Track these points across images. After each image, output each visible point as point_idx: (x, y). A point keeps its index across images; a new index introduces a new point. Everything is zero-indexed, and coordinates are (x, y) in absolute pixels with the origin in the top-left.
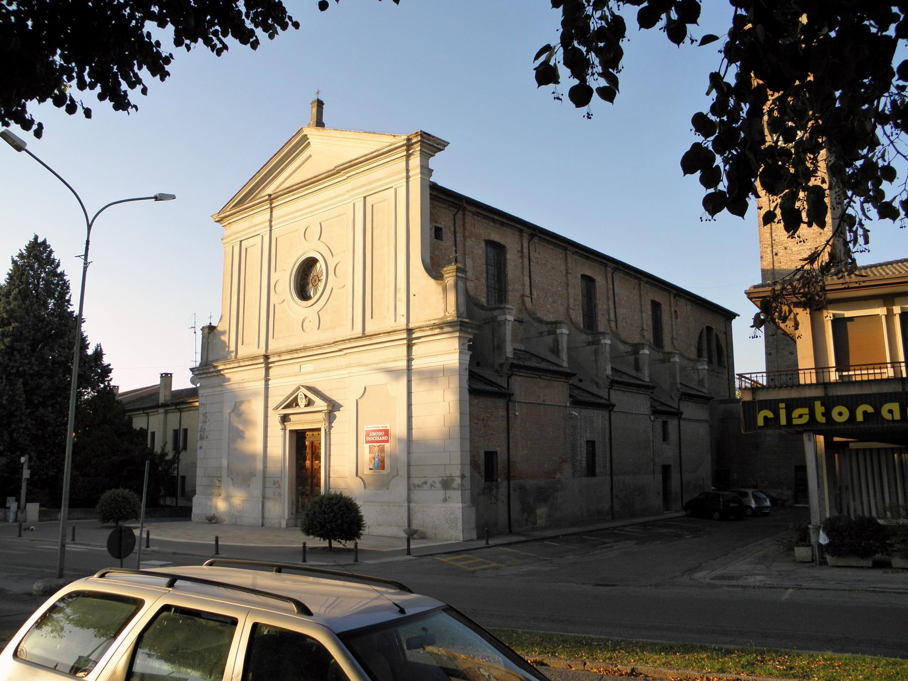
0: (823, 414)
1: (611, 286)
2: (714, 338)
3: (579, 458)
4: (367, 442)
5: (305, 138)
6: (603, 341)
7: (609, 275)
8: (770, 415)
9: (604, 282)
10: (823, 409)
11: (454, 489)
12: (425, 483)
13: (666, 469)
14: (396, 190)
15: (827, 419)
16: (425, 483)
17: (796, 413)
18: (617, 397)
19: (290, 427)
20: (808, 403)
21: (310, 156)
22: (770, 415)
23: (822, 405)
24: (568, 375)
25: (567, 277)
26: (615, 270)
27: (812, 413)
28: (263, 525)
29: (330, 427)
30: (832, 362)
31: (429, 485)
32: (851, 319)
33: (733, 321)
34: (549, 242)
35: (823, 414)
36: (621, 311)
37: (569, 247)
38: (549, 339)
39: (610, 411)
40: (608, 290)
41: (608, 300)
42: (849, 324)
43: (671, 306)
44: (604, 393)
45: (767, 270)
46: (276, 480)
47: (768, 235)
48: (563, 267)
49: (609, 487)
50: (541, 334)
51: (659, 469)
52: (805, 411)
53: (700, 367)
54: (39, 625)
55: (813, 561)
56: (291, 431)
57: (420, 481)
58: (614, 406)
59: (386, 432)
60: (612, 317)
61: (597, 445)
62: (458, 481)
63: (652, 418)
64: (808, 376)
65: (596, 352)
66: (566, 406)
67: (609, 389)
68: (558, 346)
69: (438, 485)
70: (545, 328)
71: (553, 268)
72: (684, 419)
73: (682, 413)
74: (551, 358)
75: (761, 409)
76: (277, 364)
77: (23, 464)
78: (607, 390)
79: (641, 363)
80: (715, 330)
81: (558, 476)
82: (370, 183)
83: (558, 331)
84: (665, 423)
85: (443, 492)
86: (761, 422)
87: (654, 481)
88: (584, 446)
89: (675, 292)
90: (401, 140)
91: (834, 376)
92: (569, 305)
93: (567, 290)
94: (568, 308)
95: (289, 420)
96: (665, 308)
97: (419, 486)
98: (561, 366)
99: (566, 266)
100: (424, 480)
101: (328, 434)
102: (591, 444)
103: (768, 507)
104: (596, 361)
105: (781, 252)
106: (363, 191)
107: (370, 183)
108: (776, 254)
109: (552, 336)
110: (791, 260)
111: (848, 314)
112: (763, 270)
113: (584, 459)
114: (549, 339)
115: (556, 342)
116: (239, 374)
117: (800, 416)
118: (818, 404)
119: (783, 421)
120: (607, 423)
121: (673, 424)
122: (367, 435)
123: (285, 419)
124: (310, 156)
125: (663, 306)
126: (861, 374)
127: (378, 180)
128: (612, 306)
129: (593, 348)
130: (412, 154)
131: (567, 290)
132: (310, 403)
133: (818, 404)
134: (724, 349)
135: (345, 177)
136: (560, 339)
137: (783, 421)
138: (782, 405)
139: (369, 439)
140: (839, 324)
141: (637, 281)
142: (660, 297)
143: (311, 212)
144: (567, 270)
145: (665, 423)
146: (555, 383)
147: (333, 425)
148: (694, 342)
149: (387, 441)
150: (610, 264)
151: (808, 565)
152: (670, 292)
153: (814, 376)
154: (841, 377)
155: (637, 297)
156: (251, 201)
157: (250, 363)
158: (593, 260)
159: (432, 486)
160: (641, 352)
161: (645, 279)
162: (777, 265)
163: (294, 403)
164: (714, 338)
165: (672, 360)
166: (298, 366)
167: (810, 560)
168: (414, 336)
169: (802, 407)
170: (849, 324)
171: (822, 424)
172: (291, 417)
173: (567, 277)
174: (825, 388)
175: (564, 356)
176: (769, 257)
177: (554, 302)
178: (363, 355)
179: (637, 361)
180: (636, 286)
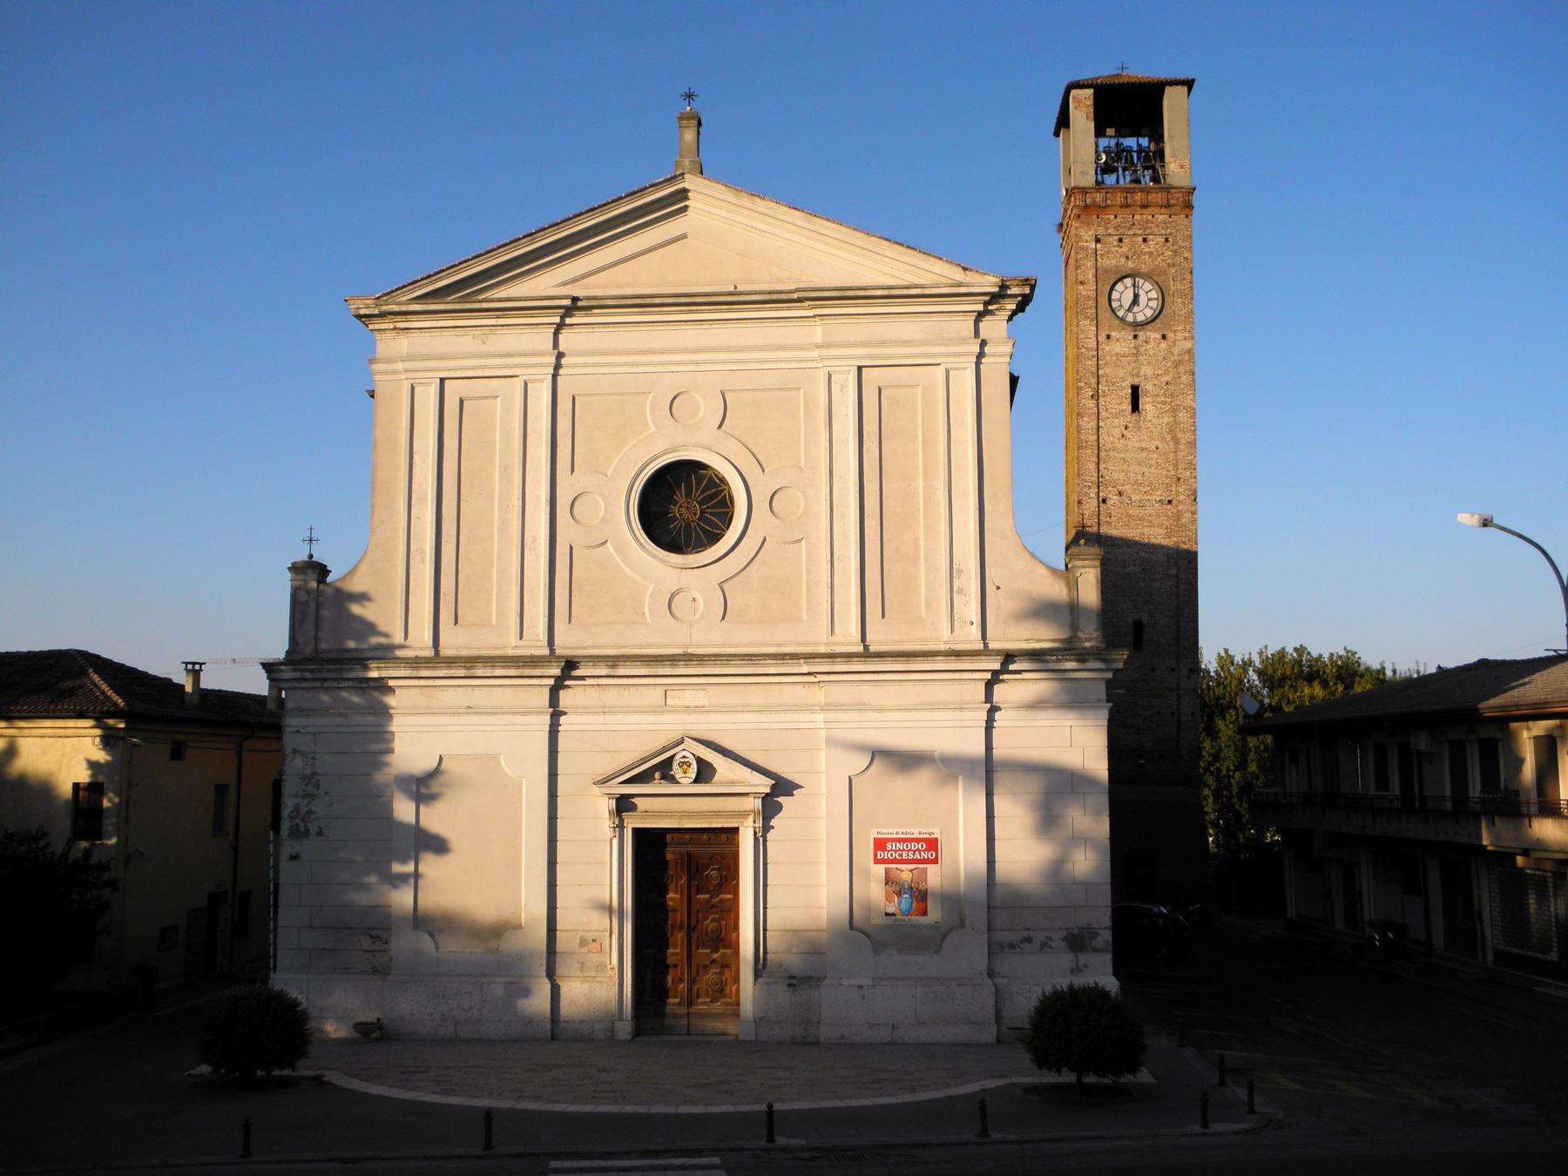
4: (877, 861)
5: (683, 194)
11: (1096, 950)
12: (1029, 940)
14: (947, 371)
16: (1029, 940)
19: (632, 822)
21: (684, 236)
28: (553, 1038)
29: (767, 828)
31: (1036, 944)
46: (589, 936)
54: (1555, 894)
56: (636, 831)
57: (1015, 937)
59: (932, 844)
62: (1107, 936)
69: (1061, 944)
76: (589, 681)
77: (1205, 798)
82: (883, 343)
85: (1072, 956)
90: (989, 284)
95: (633, 808)
97: (1011, 946)
100: (1026, 934)
101: (761, 839)
105: (1113, 499)
106: (862, 355)
107: (883, 343)
108: (1104, 501)
116: (450, 693)
122: (880, 844)
123: (624, 805)
124: (684, 236)
127: (905, 343)
130: (991, 313)
132: (705, 772)
135: (811, 313)
139: (881, 855)
143: (696, 363)
147: (772, 823)
149: (935, 861)
156: (462, 300)
157: (462, 672)
159: (1043, 945)
163: (664, 769)
166: (660, 691)
168: (1012, 667)
172: (635, 800)
176: (1091, 505)
178: (866, 688)
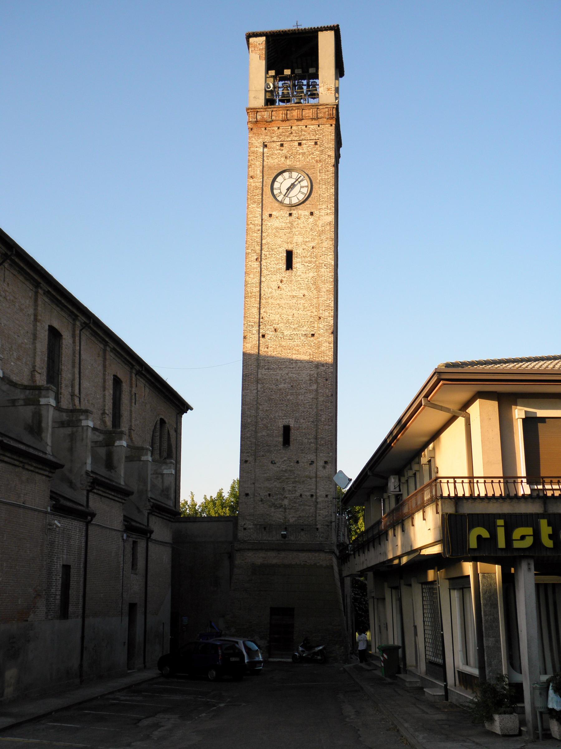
0: (550, 537)
1: (78, 348)
2: (165, 437)
3: (53, 590)
6: (84, 423)
7: (77, 332)
8: (485, 534)
9: (71, 341)
10: (549, 530)
13: (132, 607)
15: (554, 544)
17: (518, 533)
18: (96, 503)
20: (530, 520)
22: (485, 534)
23: (549, 525)
24: (53, 466)
25: (35, 326)
26: (85, 326)
27: (537, 535)
30: (522, 470)
32: (543, 420)
33: (185, 416)
34: (21, 271)
35: (550, 537)
36: (85, 384)
37: (43, 284)
38: (27, 412)
39: (88, 524)
40: (74, 353)
41: (73, 367)
42: (540, 425)
43: (131, 387)
44: (81, 497)
45: (250, 355)
47: (255, 311)
48: (31, 311)
49: (79, 635)
50: (13, 402)
51: (126, 609)
52: (529, 531)
53: (165, 472)
55: (520, 733)
58: (93, 515)
60: (77, 392)
61: (72, 570)
63: (125, 535)
64: (482, 486)
65: (72, 437)
66: (46, 513)
67: (88, 492)
68: (40, 422)
70: (20, 395)
71: (21, 310)
72: (156, 542)
73: (151, 532)
74: (28, 438)
75: (472, 527)
78: (85, 492)
79: (115, 458)
80: (167, 425)
81: (31, 617)
83: (43, 401)
84: (135, 543)
86: (473, 543)
87: (118, 625)
88: (60, 569)
89: (137, 367)
91: (524, 489)
92: (34, 367)
93: (34, 343)
94: (34, 370)
96: (125, 387)
98: (46, 454)
99: (36, 310)
102: (67, 568)
103: (260, 662)
104: (71, 450)
105: (270, 334)
108: (263, 336)
109: (32, 407)
110: (281, 346)
111: (541, 413)
112: (244, 354)
113: (59, 593)
114: (27, 412)
115: (38, 417)
117: (523, 538)
118: (543, 523)
119: (502, 544)
120: (83, 540)
121: (142, 545)
125: (124, 384)
126: (553, 490)
128: (77, 376)
129: (68, 431)
131: (34, 343)
133: (543, 523)
134: (174, 450)
136: (44, 412)
137: (502, 544)
138: (500, 522)
140: (530, 423)
141: (102, 346)
142: (122, 372)
144: (36, 315)
145: (135, 543)
146: (38, 477)
148: (149, 437)
150: (82, 318)
151: (515, 738)
152: (132, 367)
153: (466, 486)
154: (532, 490)
155: (100, 368)
158: (63, 307)
160: (117, 443)
161: (112, 344)
162: (263, 351)
164: (165, 437)
165: (143, 458)
167: (517, 732)
169: (527, 526)
170: (540, 425)
171: (547, 548)
173: (35, 326)
174: (545, 504)
175: (48, 438)
176: (253, 338)
177: (18, 359)
179: (109, 456)
180: (101, 353)
